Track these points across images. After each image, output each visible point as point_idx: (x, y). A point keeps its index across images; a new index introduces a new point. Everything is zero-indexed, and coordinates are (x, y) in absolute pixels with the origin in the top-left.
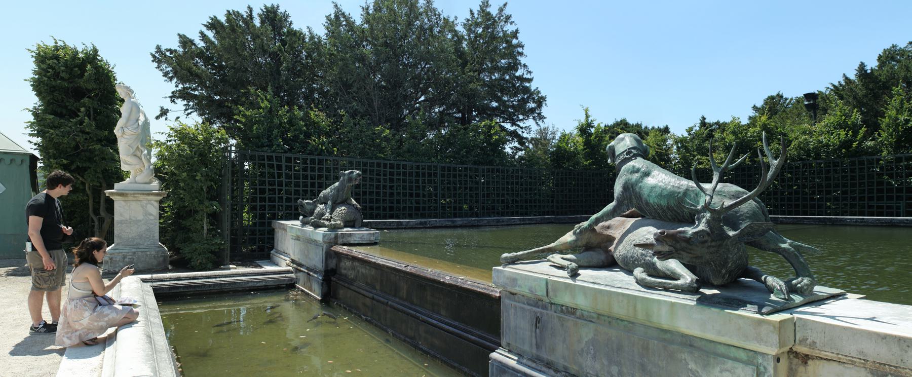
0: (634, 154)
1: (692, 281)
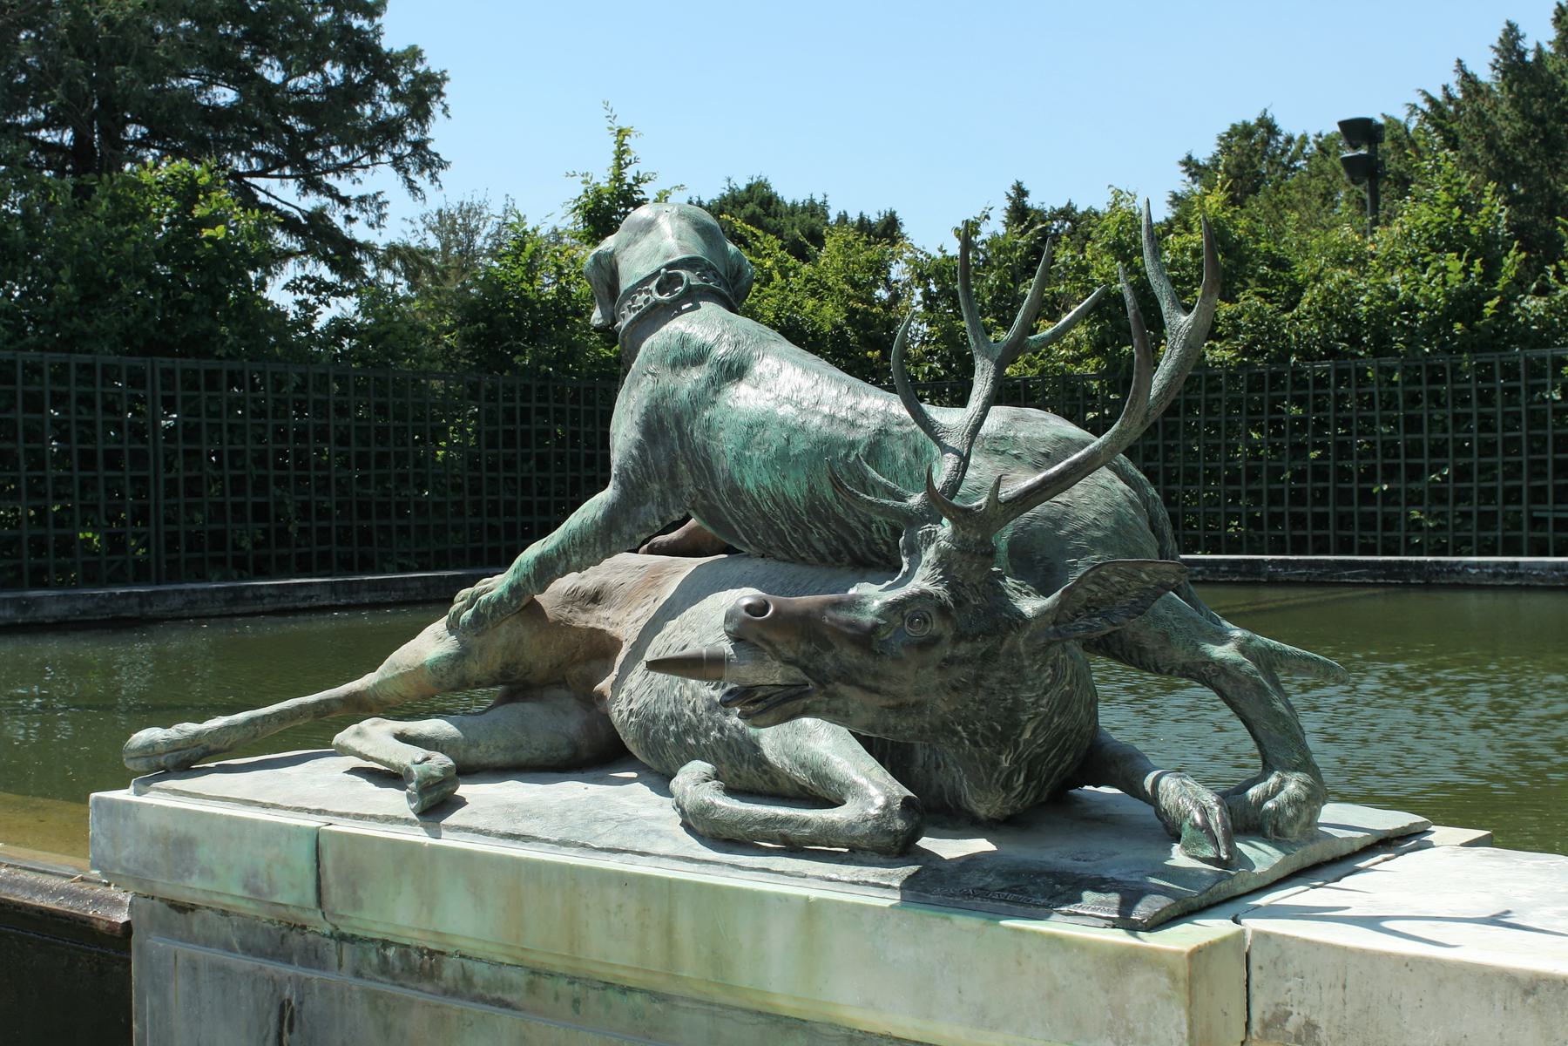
0: (689, 289)
1: (887, 806)
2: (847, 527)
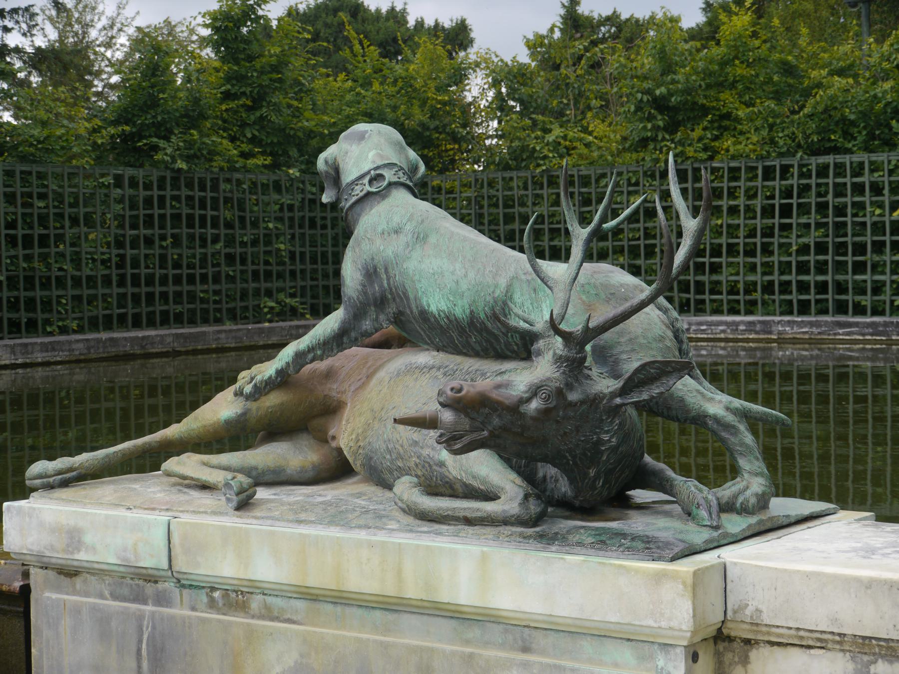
2: (492, 334)
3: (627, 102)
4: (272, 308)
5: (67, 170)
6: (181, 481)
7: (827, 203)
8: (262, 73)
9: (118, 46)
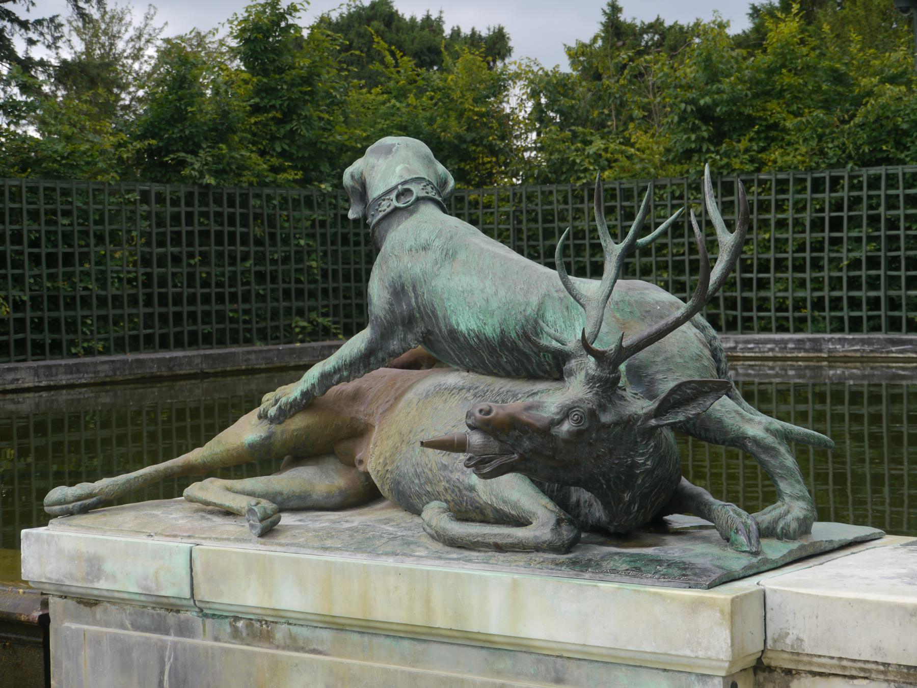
3: (671, 112)
4: (303, 328)
5: (92, 186)
6: (204, 507)
7: (879, 215)
8: (292, 85)
9: (146, 58)
